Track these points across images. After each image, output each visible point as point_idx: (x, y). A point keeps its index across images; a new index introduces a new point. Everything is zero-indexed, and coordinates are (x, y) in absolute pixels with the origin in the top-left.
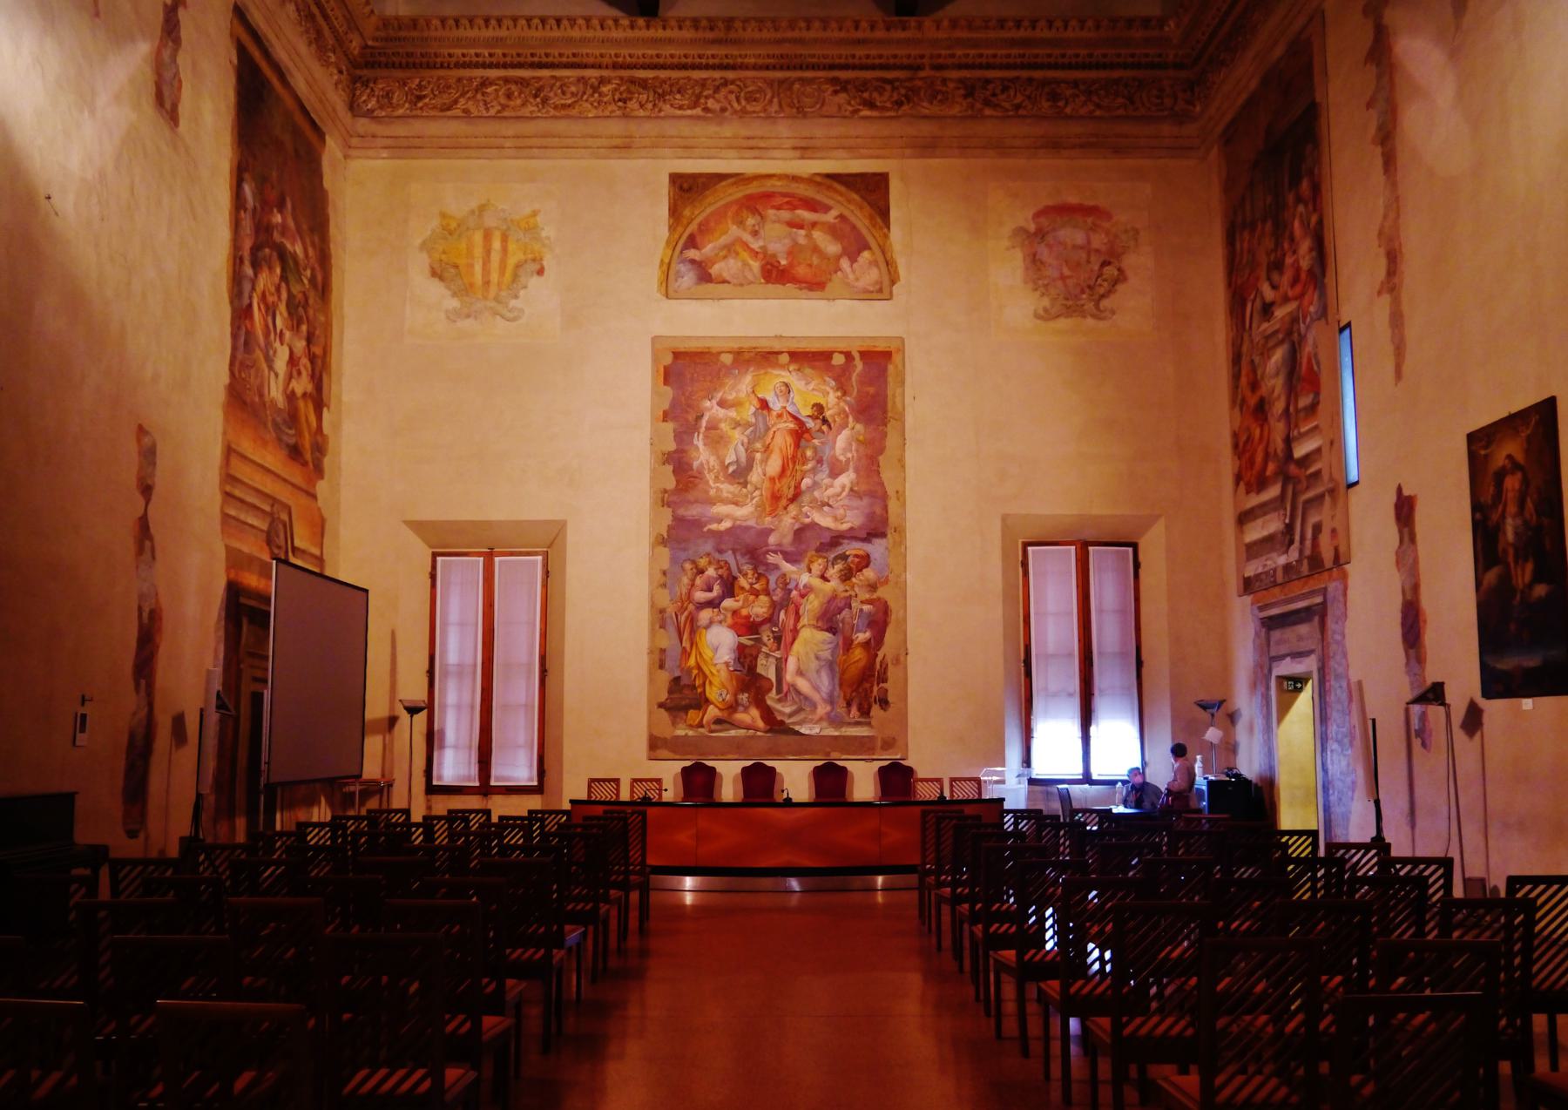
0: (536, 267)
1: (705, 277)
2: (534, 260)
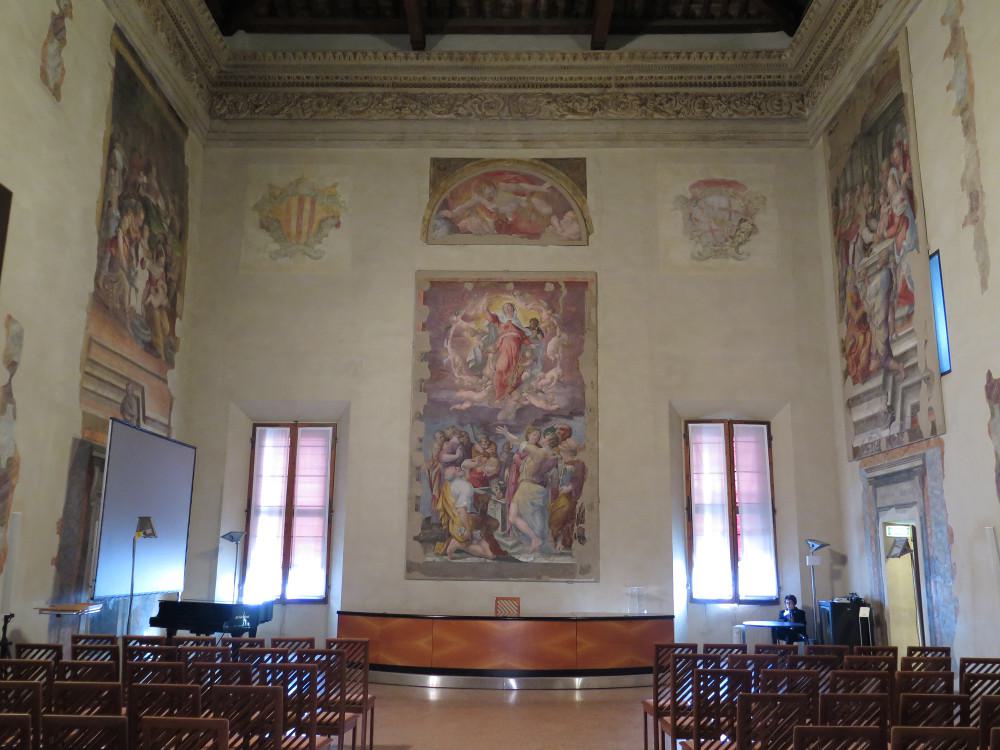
0: (333, 222)
1: (454, 228)
2: (333, 217)
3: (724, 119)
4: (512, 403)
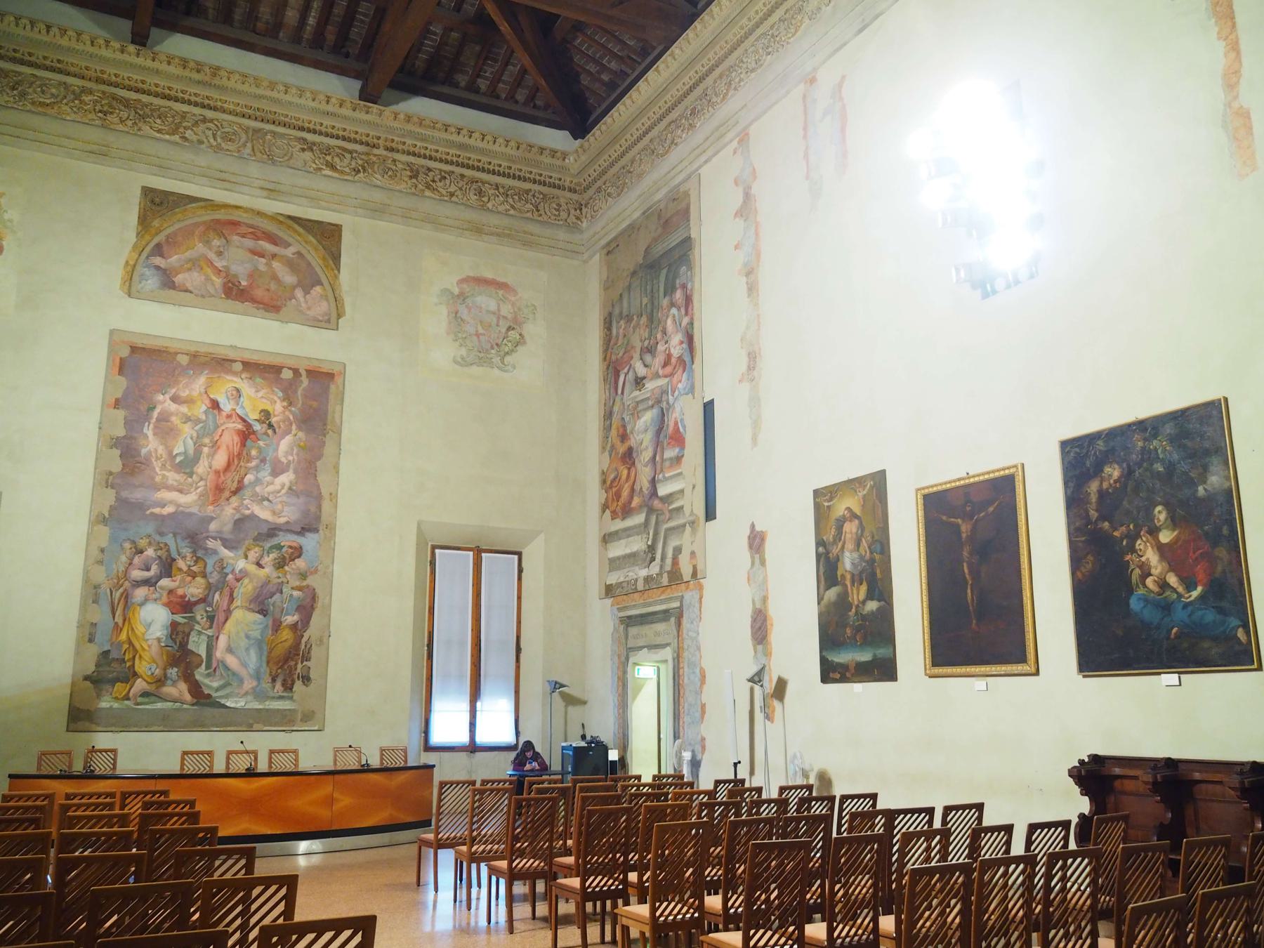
1: (168, 281)
3: (499, 212)
4: (229, 511)
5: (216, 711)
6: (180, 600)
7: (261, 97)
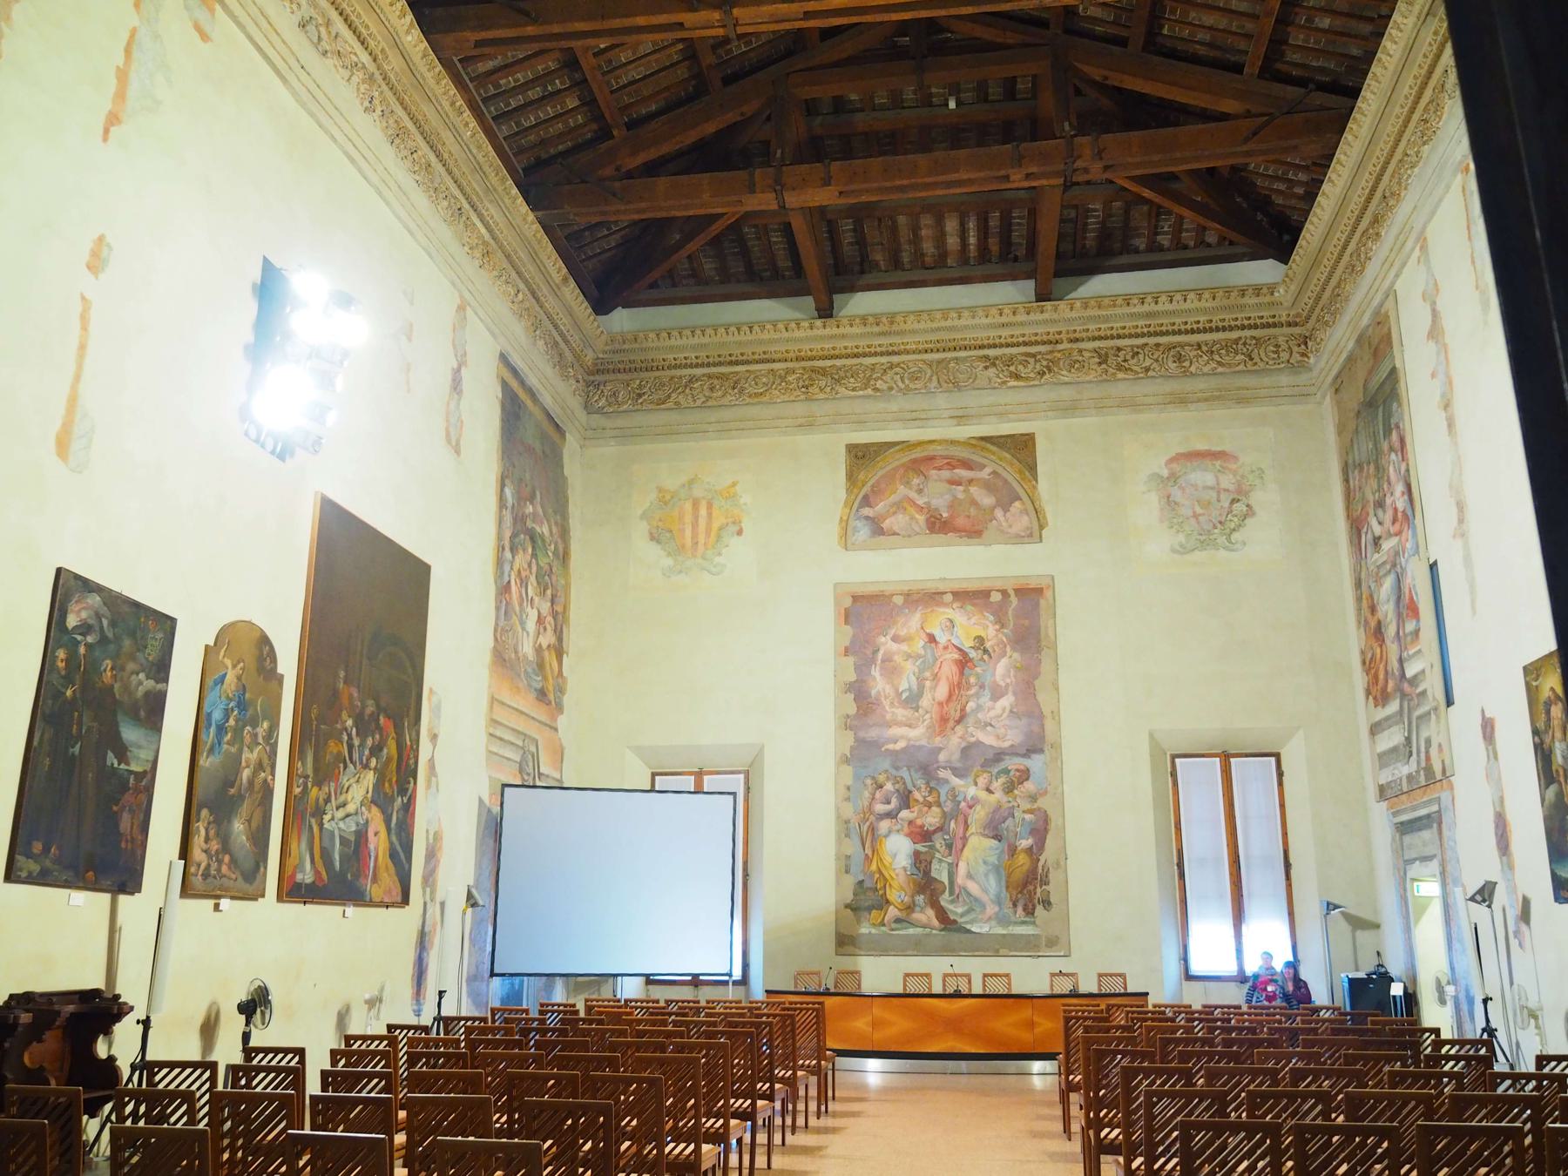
1: (878, 530)
2: (734, 523)
5: (964, 937)
6: (918, 830)
7: (938, 329)
